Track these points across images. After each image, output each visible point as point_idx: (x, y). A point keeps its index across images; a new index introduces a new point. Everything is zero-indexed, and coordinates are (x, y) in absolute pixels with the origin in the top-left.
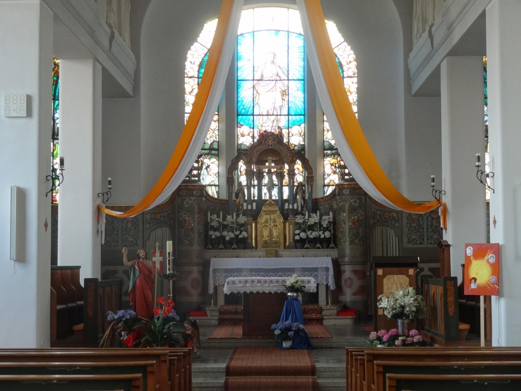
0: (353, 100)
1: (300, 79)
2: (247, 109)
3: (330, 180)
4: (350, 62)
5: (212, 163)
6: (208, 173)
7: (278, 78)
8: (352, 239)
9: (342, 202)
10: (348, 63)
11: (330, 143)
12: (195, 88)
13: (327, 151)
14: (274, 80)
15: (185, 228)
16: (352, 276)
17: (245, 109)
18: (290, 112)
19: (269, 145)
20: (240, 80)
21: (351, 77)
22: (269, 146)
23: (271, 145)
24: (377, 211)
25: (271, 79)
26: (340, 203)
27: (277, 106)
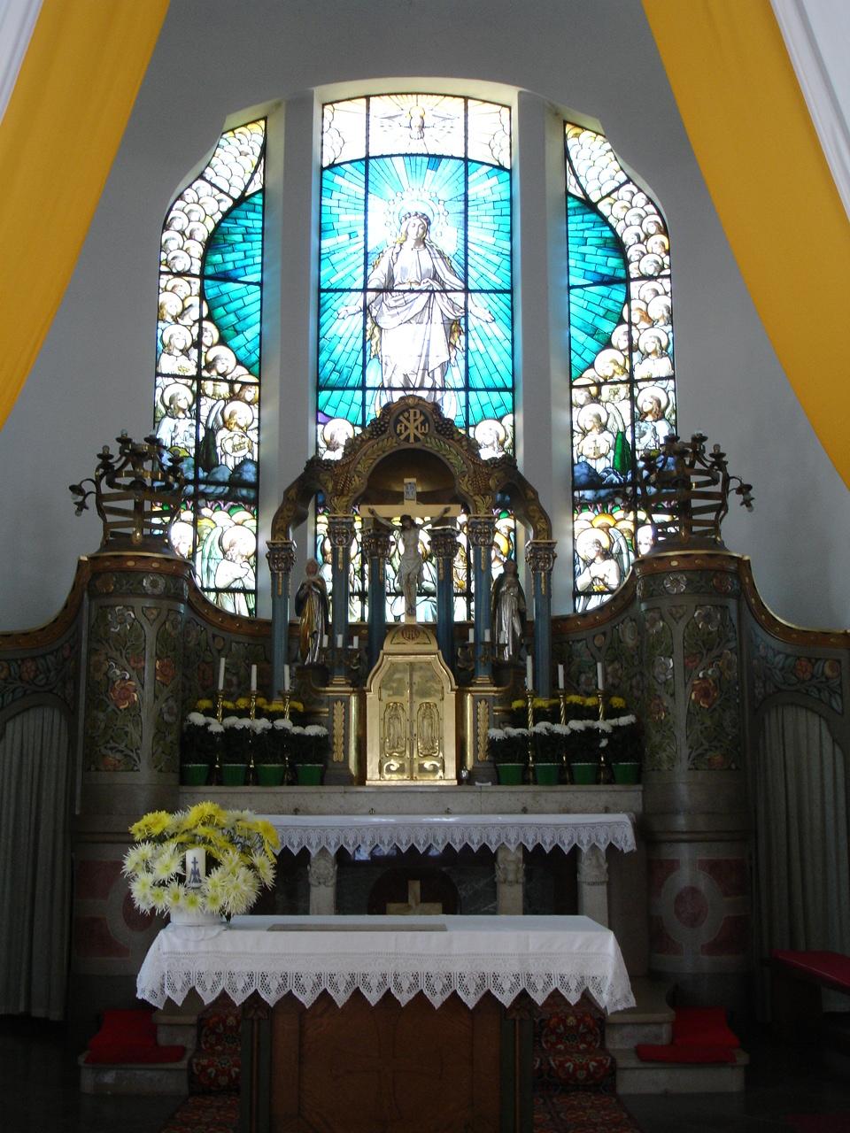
0: (659, 341)
1: (498, 288)
2: (346, 371)
3: (594, 578)
4: (648, 236)
5: (237, 524)
6: (224, 553)
7: (436, 286)
8: (699, 751)
9: (662, 618)
10: (642, 237)
11: (590, 467)
12: (191, 306)
13: (581, 492)
14: (426, 291)
15: (110, 709)
16: (704, 883)
17: (340, 373)
18: (470, 382)
19: (409, 435)
20: (328, 290)
21: (650, 278)
22: (407, 438)
23: (416, 439)
24: (775, 656)
25: (416, 287)
26: (653, 625)
27: (434, 364)
